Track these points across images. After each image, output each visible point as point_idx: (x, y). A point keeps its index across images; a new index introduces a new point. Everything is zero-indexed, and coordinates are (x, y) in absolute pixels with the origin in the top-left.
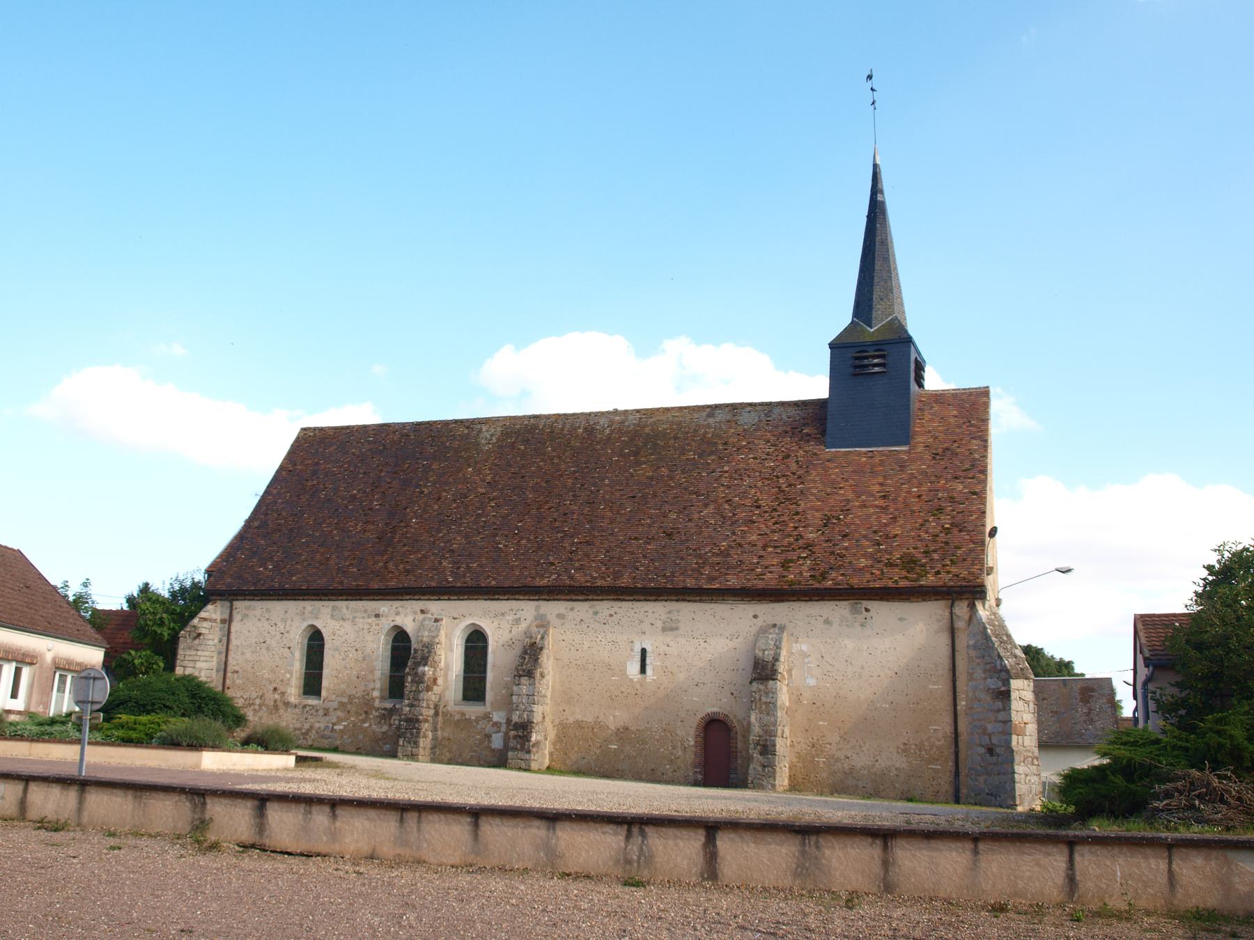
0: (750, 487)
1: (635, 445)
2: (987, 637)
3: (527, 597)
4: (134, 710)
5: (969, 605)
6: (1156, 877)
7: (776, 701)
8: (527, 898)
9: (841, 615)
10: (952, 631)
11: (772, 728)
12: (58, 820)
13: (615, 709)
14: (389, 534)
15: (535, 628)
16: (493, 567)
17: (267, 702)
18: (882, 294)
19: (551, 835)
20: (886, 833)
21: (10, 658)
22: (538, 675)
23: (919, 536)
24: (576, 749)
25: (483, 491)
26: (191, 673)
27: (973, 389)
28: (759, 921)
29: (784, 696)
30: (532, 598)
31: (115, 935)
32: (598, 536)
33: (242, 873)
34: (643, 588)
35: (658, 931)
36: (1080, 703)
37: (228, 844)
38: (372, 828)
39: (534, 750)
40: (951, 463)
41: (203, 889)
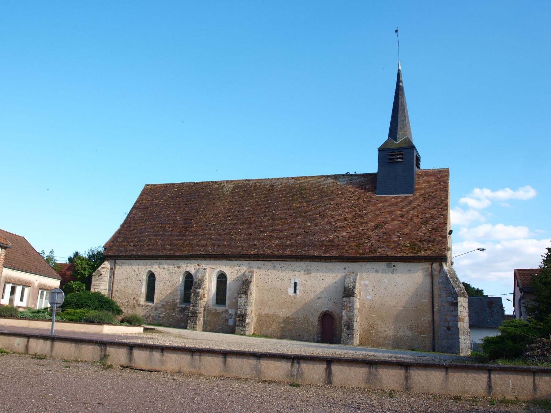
0: (343, 211)
1: (292, 193)
2: (448, 279)
3: (244, 259)
4: (74, 307)
6: (528, 385)
7: (354, 306)
8: (249, 391)
9: (383, 268)
11: (352, 318)
13: (283, 309)
14: (184, 231)
15: (248, 273)
17: (130, 304)
18: (401, 127)
21: (20, 284)
22: (249, 293)
23: (418, 234)
27: (442, 169)
28: (351, 402)
29: (357, 304)
30: (246, 260)
31: (69, 405)
32: (275, 233)
33: (123, 379)
35: (307, 407)
37: (116, 366)
38: (179, 359)
39: (247, 326)
40: (432, 202)
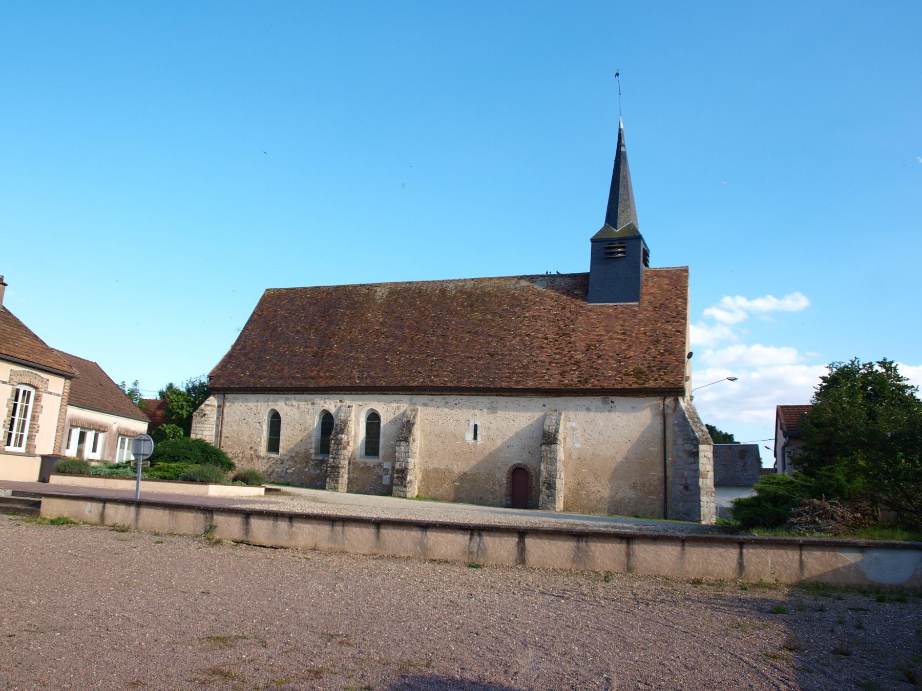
2: (685, 419)
3: (404, 393)
7: (556, 457)
10: (664, 416)
11: (553, 473)
12: (124, 525)
14: (320, 354)
16: (384, 375)
17: (246, 455)
20: (629, 536)
21: (91, 428)
22: (411, 440)
23: (645, 357)
26: (201, 437)
29: (561, 455)
30: (407, 393)
33: (236, 558)
34: (475, 388)
36: (739, 460)
38: (315, 532)
39: (409, 485)
41: (214, 567)
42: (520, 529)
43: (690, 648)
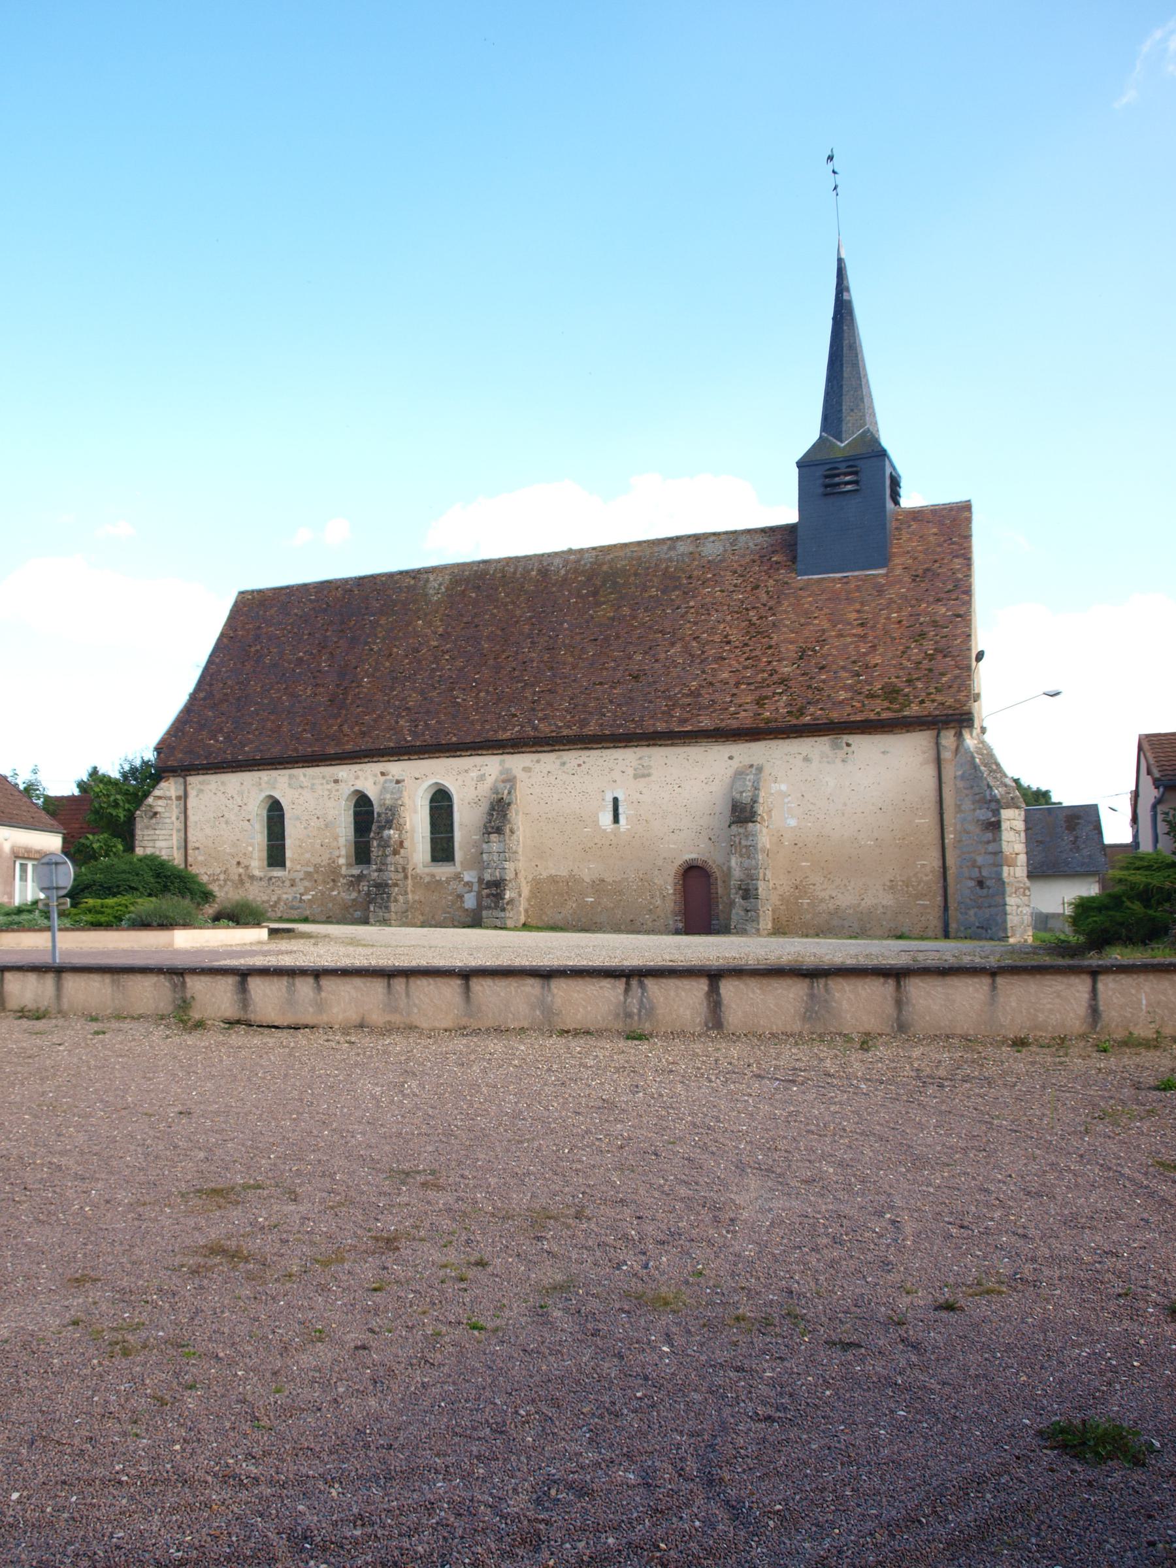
2: (975, 767)
5: (956, 733)
10: (939, 762)
11: (753, 871)
19: (546, 992)
24: (552, 904)
25: (435, 643)
38: (359, 996)
39: (509, 907)
41: (194, 1068)
42: (710, 970)
43: (1027, 1158)
